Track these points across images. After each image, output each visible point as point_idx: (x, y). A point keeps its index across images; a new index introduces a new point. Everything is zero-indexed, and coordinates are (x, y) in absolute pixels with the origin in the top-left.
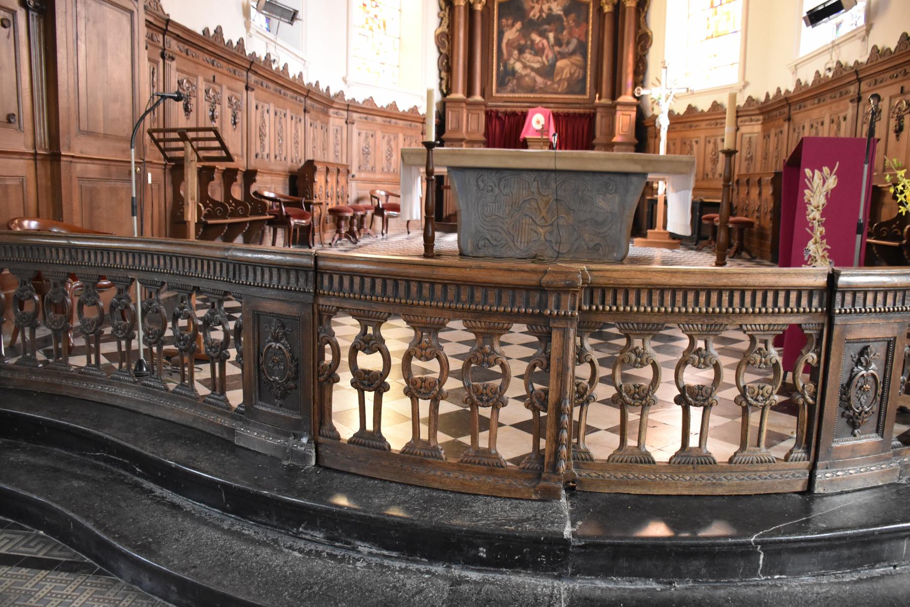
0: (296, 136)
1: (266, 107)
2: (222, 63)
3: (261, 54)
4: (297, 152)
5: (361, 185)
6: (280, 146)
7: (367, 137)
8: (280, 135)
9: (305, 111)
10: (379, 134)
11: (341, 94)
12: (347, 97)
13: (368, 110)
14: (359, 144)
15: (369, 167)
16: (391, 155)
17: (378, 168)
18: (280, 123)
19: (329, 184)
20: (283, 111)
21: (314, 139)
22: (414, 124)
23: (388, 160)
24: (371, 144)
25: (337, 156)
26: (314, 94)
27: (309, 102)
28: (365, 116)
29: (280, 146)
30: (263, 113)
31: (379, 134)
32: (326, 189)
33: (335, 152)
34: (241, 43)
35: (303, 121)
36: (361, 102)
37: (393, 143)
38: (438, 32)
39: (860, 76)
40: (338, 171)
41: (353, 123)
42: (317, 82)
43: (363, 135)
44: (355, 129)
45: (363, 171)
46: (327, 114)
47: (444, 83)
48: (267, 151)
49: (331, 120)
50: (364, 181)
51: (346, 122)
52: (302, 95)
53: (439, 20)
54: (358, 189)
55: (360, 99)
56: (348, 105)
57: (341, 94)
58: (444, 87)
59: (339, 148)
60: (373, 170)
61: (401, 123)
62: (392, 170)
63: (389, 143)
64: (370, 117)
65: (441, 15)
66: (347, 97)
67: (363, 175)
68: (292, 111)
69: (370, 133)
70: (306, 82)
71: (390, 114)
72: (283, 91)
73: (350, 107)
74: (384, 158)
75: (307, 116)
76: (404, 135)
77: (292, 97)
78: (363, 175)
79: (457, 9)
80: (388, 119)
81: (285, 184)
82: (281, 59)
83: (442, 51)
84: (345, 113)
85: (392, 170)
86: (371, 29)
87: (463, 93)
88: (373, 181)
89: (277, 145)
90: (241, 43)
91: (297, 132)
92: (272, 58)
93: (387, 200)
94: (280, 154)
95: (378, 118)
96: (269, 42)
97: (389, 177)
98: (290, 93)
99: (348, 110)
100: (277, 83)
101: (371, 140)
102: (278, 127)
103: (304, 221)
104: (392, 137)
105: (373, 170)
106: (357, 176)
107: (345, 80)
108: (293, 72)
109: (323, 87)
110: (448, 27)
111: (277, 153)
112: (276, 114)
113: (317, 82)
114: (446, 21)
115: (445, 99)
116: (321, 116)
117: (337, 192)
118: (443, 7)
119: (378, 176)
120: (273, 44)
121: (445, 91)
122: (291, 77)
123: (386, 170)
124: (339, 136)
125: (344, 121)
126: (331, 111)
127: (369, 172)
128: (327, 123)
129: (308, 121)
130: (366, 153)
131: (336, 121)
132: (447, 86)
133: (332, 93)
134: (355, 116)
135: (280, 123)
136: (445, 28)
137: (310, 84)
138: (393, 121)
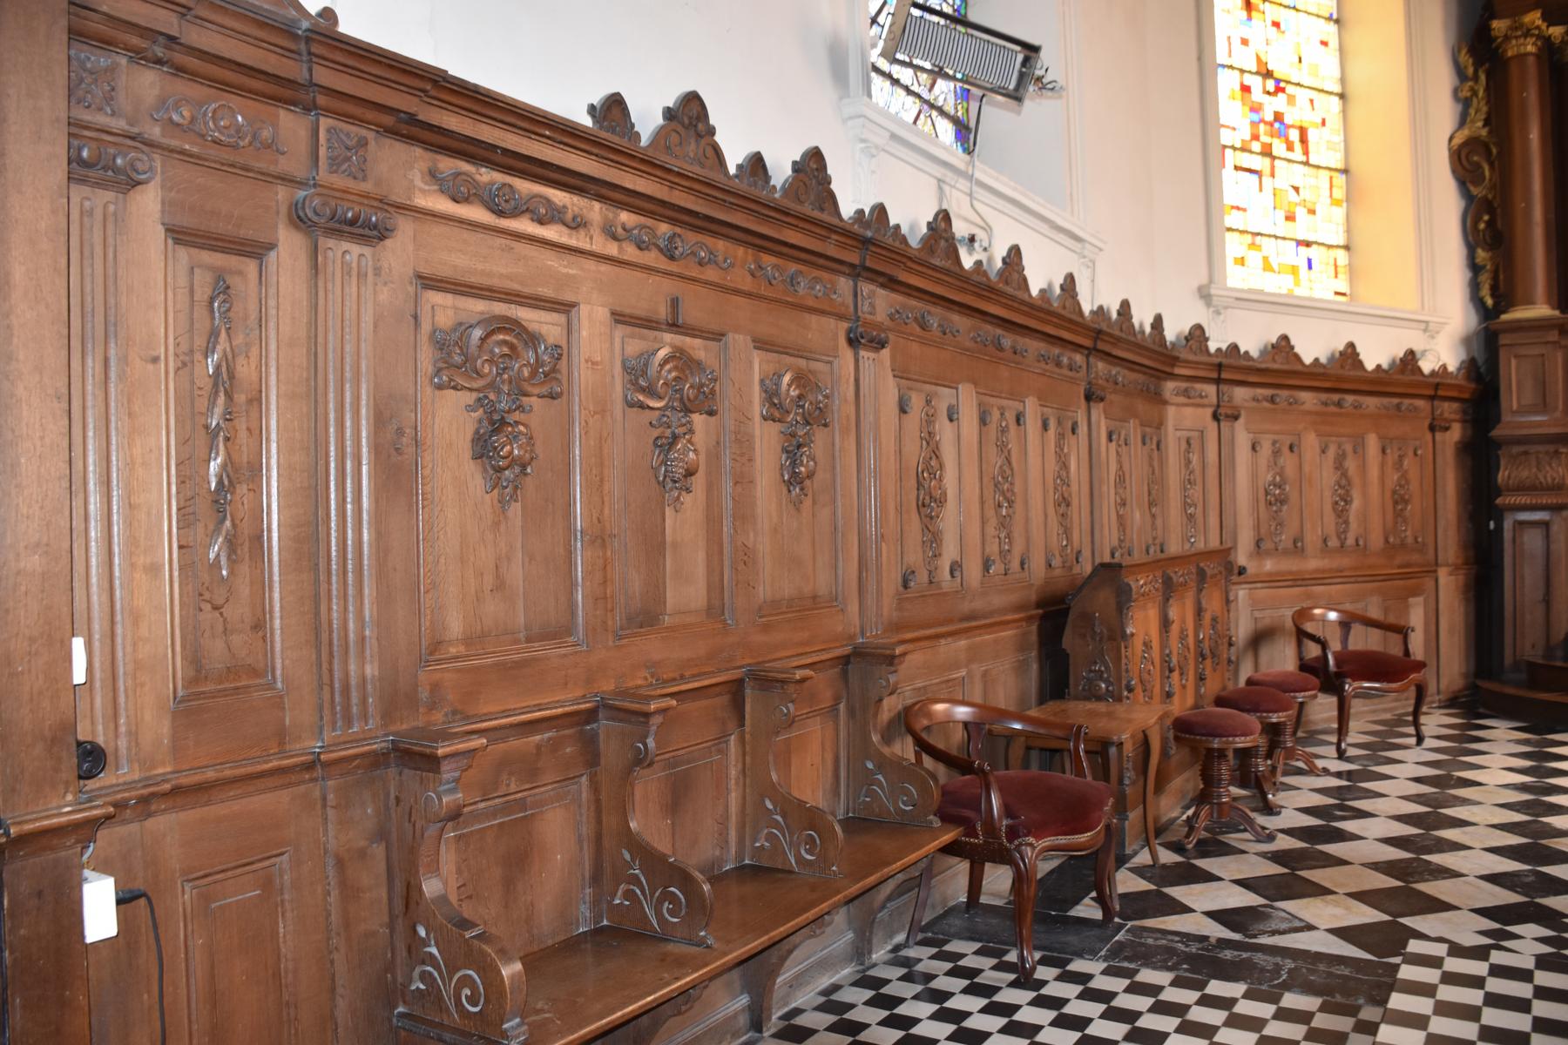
0: (1063, 479)
1: (945, 397)
2: (721, 245)
3: (911, 216)
4: (1067, 532)
5: (1263, 593)
6: (1004, 523)
7: (1276, 453)
8: (1001, 490)
9: (1089, 397)
10: (1311, 441)
11: (1197, 335)
12: (1217, 342)
13: (1278, 371)
14: (1254, 476)
15: (1285, 539)
16: (1347, 500)
17: (1312, 539)
18: (1002, 447)
19: (1175, 628)
20: (1013, 406)
21: (1121, 480)
22: (1407, 401)
23: (1341, 513)
24: (1290, 471)
25: (1191, 517)
26: (1117, 341)
27: (1101, 366)
28: (1268, 392)
29: (1004, 523)
30: (930, 419)
31: (1311, 441)
32: (1164, 643)
33: (1186, 505)
34: (812, 166)
35: (1083, 429)
36: (1254, 353)
37: (1351, 464)
38: (1457, 141)
39: (1224, 376)
40: (1201, 574)
41: (1236, 418)
42: (1125, 306)
43: (1266, 449)
44: (1241, 435)
45: (1268, 553)
46: (1158, 400)
47: (1485, 278)
48: (950, 552)
49: (1171, 411)
50: (1272, 580)
51: (1216, 417)
52: (1078, 347)
53: (1459, 107)
54: (1255, 604)
55: (1251, 345)
56: (1220, 366)
57: (1197, 335)
58: (1485, 292)
59: (1196, 493)
60: (1297, 547)
61: (1371, 403)
62: (1350, 541)
63: (1339, 465)
64: (1284, 393)
65: (1466, 93)
66: (1217, 342)
67: (1269, 565)
68: (1043, 399)
69: (1288, 440)
70: (1087, 308)
71: (1342, 376)
72: (1008, 341)
73: (1229, 369)
74: (1328, 508)
75: (1097, 411)
76: (1381, 438)
77: (1043, 358)
78: (1269, 565)
79: (1514, 69)
80: (1336, 397)
81: (1022, 647)
82: (991, 234)
83: (1474, 191)
84: (1211, 389)
85: (1350, 541)
86: (1267, 152)
87: (1549, 302)
88: (1298, 580)
89: (993, 522)
90: (812, 166)
91: (1065, 466)
92: (960, 229)
93: (1345, 640)
94: (1004, 554)
95: (1305, 396)
96: (949, 176)
97: (1345, 562)
98: (1033, 346)
99: (1218, 381)
100: (983, 314)
101: (1288, 461)
102: (994, 459)
103: (1083, 838)
104: (1348, 448)
105: (1297, 547)
106: (1252, 568)
107: (1205, 295)
108: (1040, 276)
109: (1142, 318)
110: (1487, 122)
111: (992, 549)
112: (983, 421)
113: (1125, 306)
114: (1480, 108)
115: (1494, 324)
116: (1141, 406)
117: (1198, 642)
118: (1471, 70)
119: (1313, 564)
120: (963, 184)
121: (1489, 302)
122: (1034, 292)
123: (1333, 543)
124: (1195, 458)
125: (1209, 411)
126: (1170, 386)
127: (1286, 552)
128: (1160, 425)
129: (1102, 426)
130: (1274, 499)
131: (1184, 417)
132: (1494, 290)
133: (1170, 334)
134: (1241, 394)
135: (1002, 447)
136: (1478, 128)
137: (1100, 312)
138: (1350, 399)
